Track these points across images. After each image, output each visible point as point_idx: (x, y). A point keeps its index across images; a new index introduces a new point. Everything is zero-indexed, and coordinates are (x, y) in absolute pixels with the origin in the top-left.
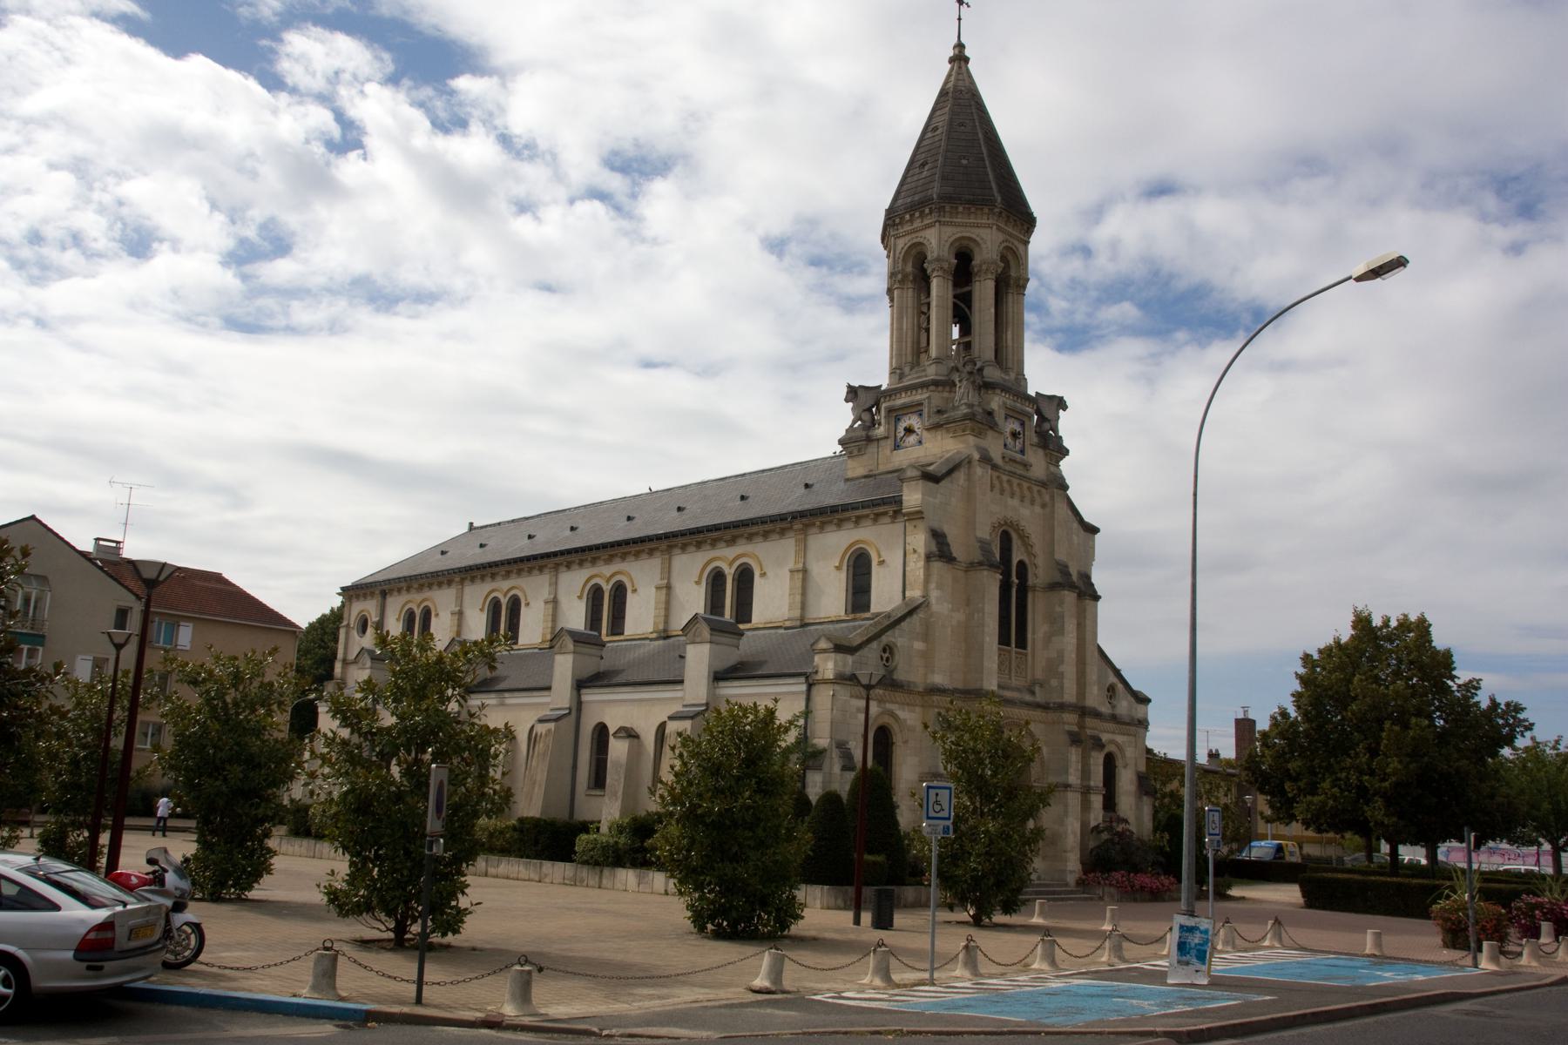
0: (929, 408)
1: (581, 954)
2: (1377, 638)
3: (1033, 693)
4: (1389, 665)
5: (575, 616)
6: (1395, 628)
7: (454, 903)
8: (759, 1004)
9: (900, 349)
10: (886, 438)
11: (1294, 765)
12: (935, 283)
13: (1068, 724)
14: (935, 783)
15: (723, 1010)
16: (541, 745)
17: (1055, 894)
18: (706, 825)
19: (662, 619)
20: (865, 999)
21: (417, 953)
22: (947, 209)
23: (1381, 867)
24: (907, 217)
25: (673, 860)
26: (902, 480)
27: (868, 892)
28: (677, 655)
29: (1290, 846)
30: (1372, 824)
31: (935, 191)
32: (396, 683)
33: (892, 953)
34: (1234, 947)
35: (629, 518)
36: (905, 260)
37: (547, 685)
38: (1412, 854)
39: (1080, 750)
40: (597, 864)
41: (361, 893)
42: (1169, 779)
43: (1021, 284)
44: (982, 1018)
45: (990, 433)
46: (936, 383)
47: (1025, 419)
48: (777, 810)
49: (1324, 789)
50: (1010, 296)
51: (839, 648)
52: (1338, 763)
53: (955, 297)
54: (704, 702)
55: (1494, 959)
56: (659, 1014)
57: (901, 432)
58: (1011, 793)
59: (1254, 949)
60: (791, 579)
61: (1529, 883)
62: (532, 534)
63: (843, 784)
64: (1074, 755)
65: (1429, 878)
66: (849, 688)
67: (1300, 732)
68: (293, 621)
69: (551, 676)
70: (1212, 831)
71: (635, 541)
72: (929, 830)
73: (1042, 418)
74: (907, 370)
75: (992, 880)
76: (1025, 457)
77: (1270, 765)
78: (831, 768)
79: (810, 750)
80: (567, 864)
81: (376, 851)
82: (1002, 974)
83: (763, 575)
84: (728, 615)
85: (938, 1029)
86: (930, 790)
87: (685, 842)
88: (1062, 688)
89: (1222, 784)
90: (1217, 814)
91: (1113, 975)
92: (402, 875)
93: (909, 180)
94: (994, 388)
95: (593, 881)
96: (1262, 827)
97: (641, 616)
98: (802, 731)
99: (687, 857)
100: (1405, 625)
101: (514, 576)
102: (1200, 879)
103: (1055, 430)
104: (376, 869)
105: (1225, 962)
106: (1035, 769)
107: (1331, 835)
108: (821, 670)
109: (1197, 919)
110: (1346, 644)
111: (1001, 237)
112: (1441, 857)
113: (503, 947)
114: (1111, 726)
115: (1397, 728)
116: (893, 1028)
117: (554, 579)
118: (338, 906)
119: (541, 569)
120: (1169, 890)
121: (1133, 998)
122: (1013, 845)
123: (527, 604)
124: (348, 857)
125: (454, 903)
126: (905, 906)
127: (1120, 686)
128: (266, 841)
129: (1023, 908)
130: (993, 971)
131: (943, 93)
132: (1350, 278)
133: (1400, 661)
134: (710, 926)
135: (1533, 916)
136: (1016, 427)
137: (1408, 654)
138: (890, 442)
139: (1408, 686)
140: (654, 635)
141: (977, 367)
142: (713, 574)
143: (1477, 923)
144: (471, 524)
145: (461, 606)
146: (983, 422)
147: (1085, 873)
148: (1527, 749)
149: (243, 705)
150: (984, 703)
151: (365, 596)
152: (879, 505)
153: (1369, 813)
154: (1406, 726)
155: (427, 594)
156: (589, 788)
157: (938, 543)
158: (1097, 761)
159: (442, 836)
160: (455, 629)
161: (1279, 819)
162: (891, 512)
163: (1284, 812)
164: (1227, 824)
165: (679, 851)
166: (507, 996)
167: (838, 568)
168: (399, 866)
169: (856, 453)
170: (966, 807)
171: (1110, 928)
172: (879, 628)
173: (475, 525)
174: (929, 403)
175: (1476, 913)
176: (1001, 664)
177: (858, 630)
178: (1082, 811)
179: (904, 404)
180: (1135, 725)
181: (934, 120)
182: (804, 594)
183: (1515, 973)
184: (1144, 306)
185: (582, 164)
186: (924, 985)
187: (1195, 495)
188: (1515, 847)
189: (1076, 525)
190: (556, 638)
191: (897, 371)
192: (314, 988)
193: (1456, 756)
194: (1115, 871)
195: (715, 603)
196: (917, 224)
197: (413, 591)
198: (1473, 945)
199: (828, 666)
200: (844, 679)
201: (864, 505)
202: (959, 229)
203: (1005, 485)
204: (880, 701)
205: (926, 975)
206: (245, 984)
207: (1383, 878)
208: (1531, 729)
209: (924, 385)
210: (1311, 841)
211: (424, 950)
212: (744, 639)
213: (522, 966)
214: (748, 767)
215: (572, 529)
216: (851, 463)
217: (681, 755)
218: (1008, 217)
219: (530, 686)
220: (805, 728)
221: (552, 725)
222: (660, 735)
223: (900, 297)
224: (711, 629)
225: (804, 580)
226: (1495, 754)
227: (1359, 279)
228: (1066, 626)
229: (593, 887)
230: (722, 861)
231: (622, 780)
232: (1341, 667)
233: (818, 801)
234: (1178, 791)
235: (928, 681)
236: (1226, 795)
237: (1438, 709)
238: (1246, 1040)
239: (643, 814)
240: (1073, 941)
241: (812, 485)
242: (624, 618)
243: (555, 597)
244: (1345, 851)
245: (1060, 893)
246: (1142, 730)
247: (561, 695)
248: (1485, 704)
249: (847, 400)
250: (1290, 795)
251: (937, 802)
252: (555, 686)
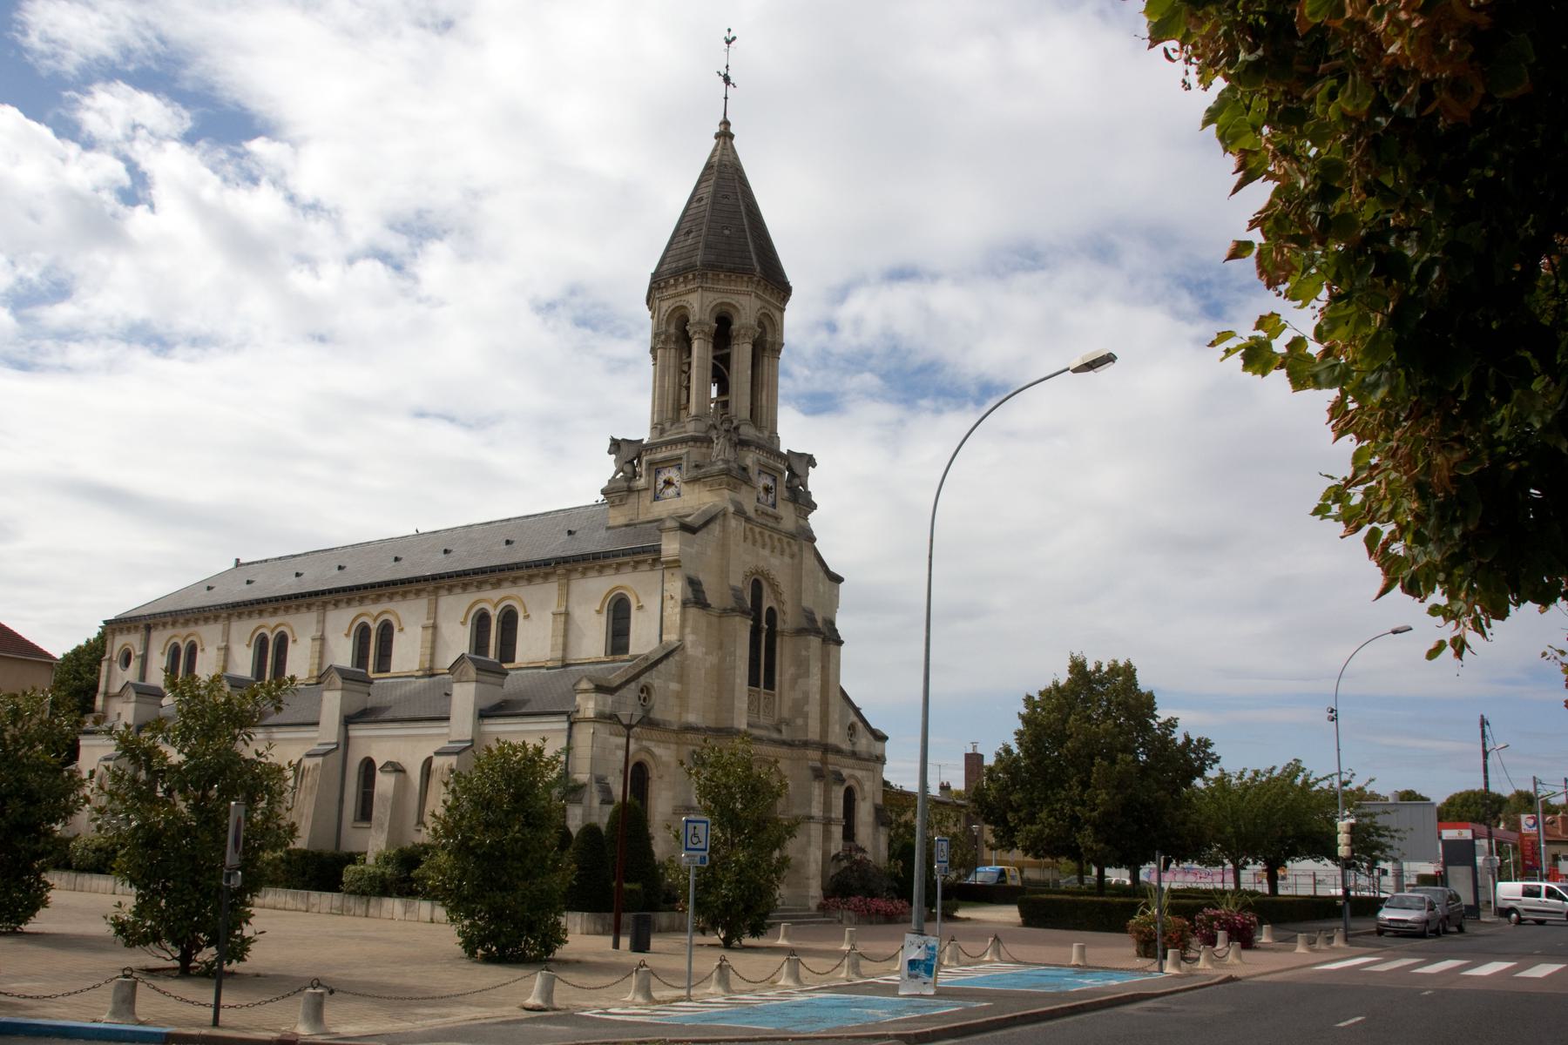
0: (688, 462)
1: (359, 979)
2: (1090, 681)
3: (780, 731)
4: (1100, 706)
5: (342, 653)
6: (1106, 673)
7: (238, 932)
8: (533, 1020)
9: (661, 405)
10: (647, 489)
11: (1015, 797)
12: (696, 345)
13: (812, 760)
14: (692, 817)
15: (501, 1026)
16: (309, 779)
17: (799, 919)
18: (477, 857)
19: (428, 658)
20: (629, 1014)
21: (214, 981)
22: (710, 275)
23: (1090, 888)
24: (672, 281)
25: (445, 889)
26: (661, 531)
27: (627, 918)
28: (443, 692)
29: (1011, 870)
30: (1082, 850)
31: (698, 258)
32: (185, 722)
33: (652, 972)
34: (958, 961)
35: (397, 559)
36: (668, 323)
37: (315, 720)
38: (1118, 876)
39: (822, 784)
40: (364, 894)
41: (148, 923)
42: (904, 811)
43: (777, 348)
44: (735, 1028)
45: (744, 488)
46: (695, 439)
47: (777, 475)
48: (544, 842)
49: (1041, 819)
50: (766, 359)
51: (600, 689)
52: (1054, 795)
53: (715, 358)
54: (470, 738)
55: (1176, 965)
56: (442, 1031)
57: (661, 484)
58: (760, 826)
59: (976, 964)
60: (554, 621)
61: (1211, 898)
62: (300, 572)
63: (602, 817)
64: (817, 790)
65: (1130, 896)
66: (608, 726)
67: (1021, 767)
68: (50, 652)
69: (319, 712)
70: (940, 859)
71: (403, 582)
72: (687, 860)
73: (793, 474)
74: (667, 425)
75: (742, 906)
76: (776, 511)
77: (994, 798)
78: (591, 801)
79: (571, 784)
80: (335, 894)
81: (164, 883)
82: (753, 991)
83: (527, 617)
84: (492, 655)
85: (698, 1038)
86: (689, 824)
87: (457, 872)
88: (807, 725)
89: (952, 814)
90: (945, 843)
91: (851, 988)
92: (190, 906)
93: (674, 246)
94: (749, 446)
95: (360, 910)
96: (987, 854)
97: (407, 654)
98: (563, 767)
99: (459, 887)
100: (1114, 670)
101: (281, 612)
102: (929, 902)
103: (805, 485)
104: (164, 901)
105: (951, 975)
106: (781, 804)
107: (1048, 860)
108: (582, 709)
109: (925, 938)
110: (1064, 687)
111: (758, 304)
112: (1143, 877)
113: (286, 973)
114: (851, 762)
115: (1105, 763)
116: (657, 1038)
117: (321, 618)
118: (126, 937)
119: (309, 607)
120: (902, 913)
121: (868, 1007)
122: (762, 874)
123: (295, 641)
124: (134, 889)
125: (238, 932)
126: (660, 931)
127: (860, 725)
128: (43, 875)
129: (768, 931)
130: (743, 988)
131: (709, 166)
132: (1068, 369)
133: (1110, 702)
134: (480, 951)
135: (1212, 927)
136: (769, 483)
137: (1117, 697)
138: (650, 494)
139: (1116, 725)
140: (420, 673)
141: (734, 425)
142: (477, 616)
143: (1164, 934)
144: (238, 560)
145: (228, 641)
146: (738, 477)
147: (826, 897)
148: (1216, 780)
149: (22, 742)
150: (737, 741)
151: (129, 630)
152: (639, 553)
153: (1079, 841)
154: (1113, 762)
155: (192, 629)
156: (355, 820)
157: (693, 590)
158: (838, 794)
159: (238, 869)
160: (221, 664)
161: (1002, 847)
162: (650, 561)
163: (1006, 840)
164: (956, 851)
165: (451, 879)
166: (300, 1017)
167: (599, 612)
168: (187, 898)
169: (617, 502)
170: (718, 838)
171: (849, 948)
172: (637, 670)
173: (241, 561)
174: (688, 457)
175: (1163, 926)
176: (750, 703)
177: (618, 671)
178: (823, 842)
179: (664, 458)
180: (874, 761)
181: (700, 191)
182: (566, 635)
183: (1192, 975)
184: (885, 377)
185: (363, 227)
186: (682, 1001)
187: (930, 557)
188: (1203, 867)
189: (822, 574)
190: (322, 678)
191: (658, 427)
192: (114, 1013)
193: (1155, 787)
194: (854, 896)
195: (480, 643)
196: (681, 288)
197: (179, 625)
198: (1159, 953)
199: (588, 705)
200: (603, 718)
201: (624, 553)
202: (719, 295)
203: (757, 536)
204: (637, 739)
205: (683, 993)
206: (41, 1012)
207: (1090, 898)
208: (1218, 762)
209: (683, 441)
210: (1031, 866)
211: (215, 976)
212: (508, 678)
213: (314, 988)
214: (517, 802)
215: (340, 568)
216: (612, 512)
217: (454, 791)
218: (766, 286)
219: (298, 721)
220: (567, 764)
221: (319, 760)
222: (426, 767)
223: (663, 356)
224: (477, 669)
225: (567, 622)
226: (1188, 785)
227: (1075, 371)
228: (811, 668)
229: (360, 916)
230: (491, 889)
231: (389, 812)
232: (1059, 708)
233: (579, 832)
234: (912, 822)
235: (683, 720)
236: (955, 825)
237: (1141, 745)
238: (964, 1040)
239: (409, 845)
240: (816, 960)
241: (575, 532)
242: (390, 656)
243: (323, 635)
244: (1061, 875)
245: (803, 917)
246: (879, 765)
247: (329, 730)
248: (1180, 741)
249: (610, 452)
250: (1012, 825)
251: (695, 835)
252: (323, 721)
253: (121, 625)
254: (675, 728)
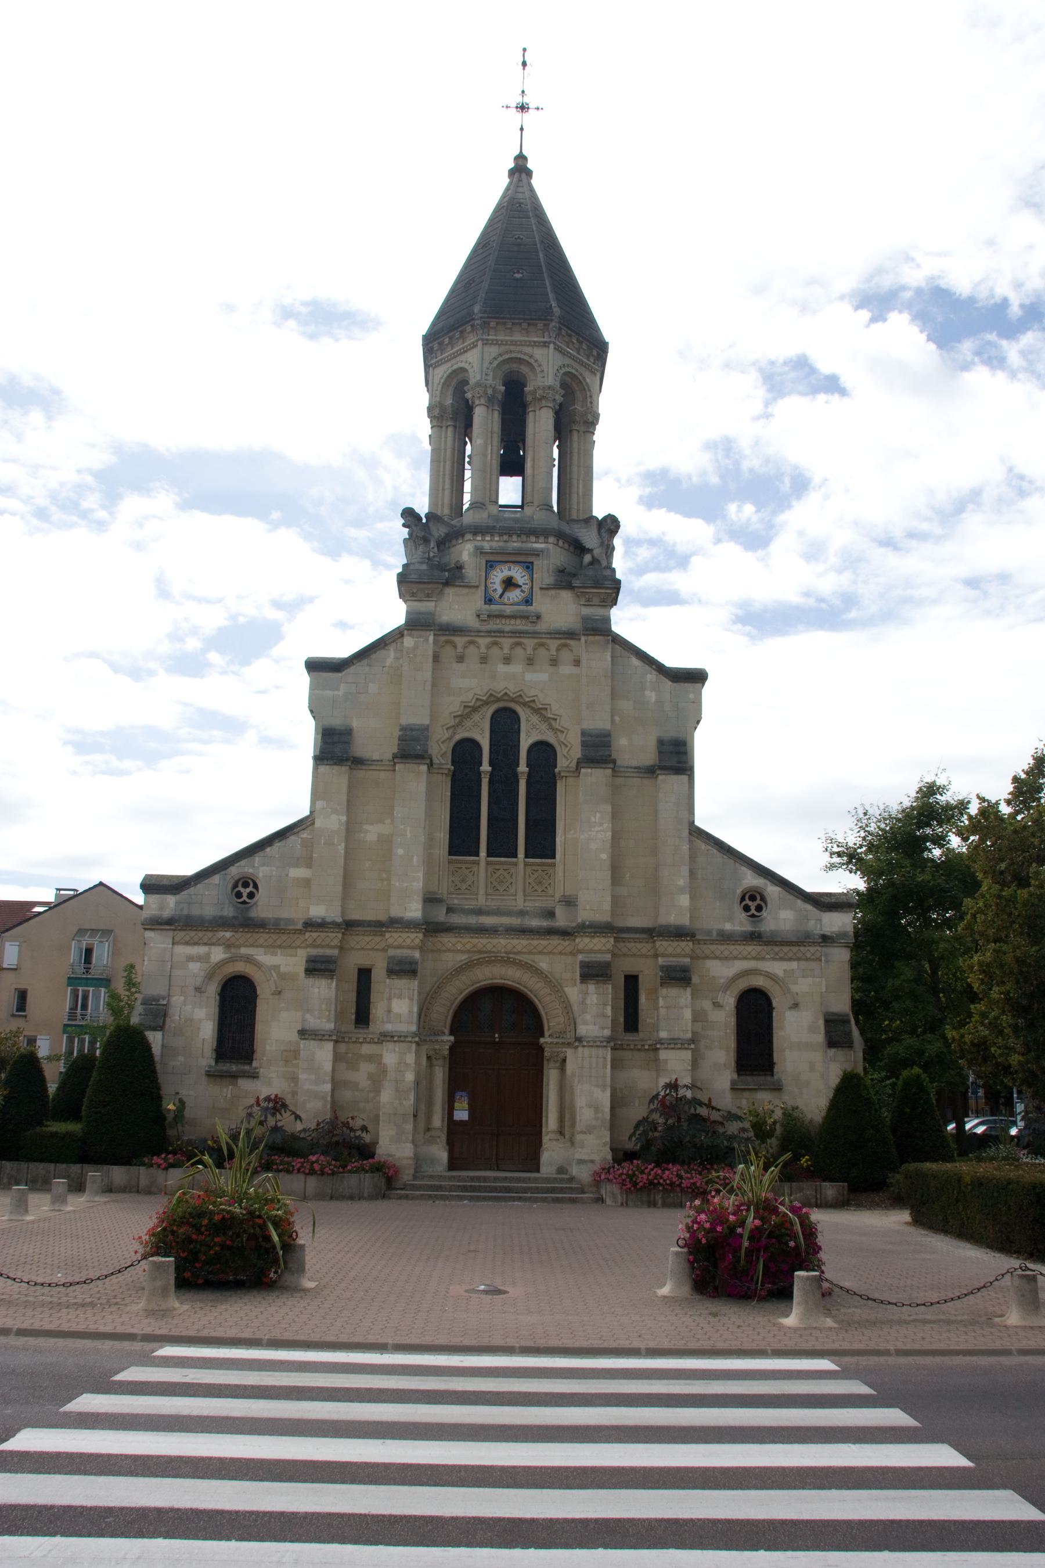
66: (171, 933)
94: (463, 536)
254: (300, 926)
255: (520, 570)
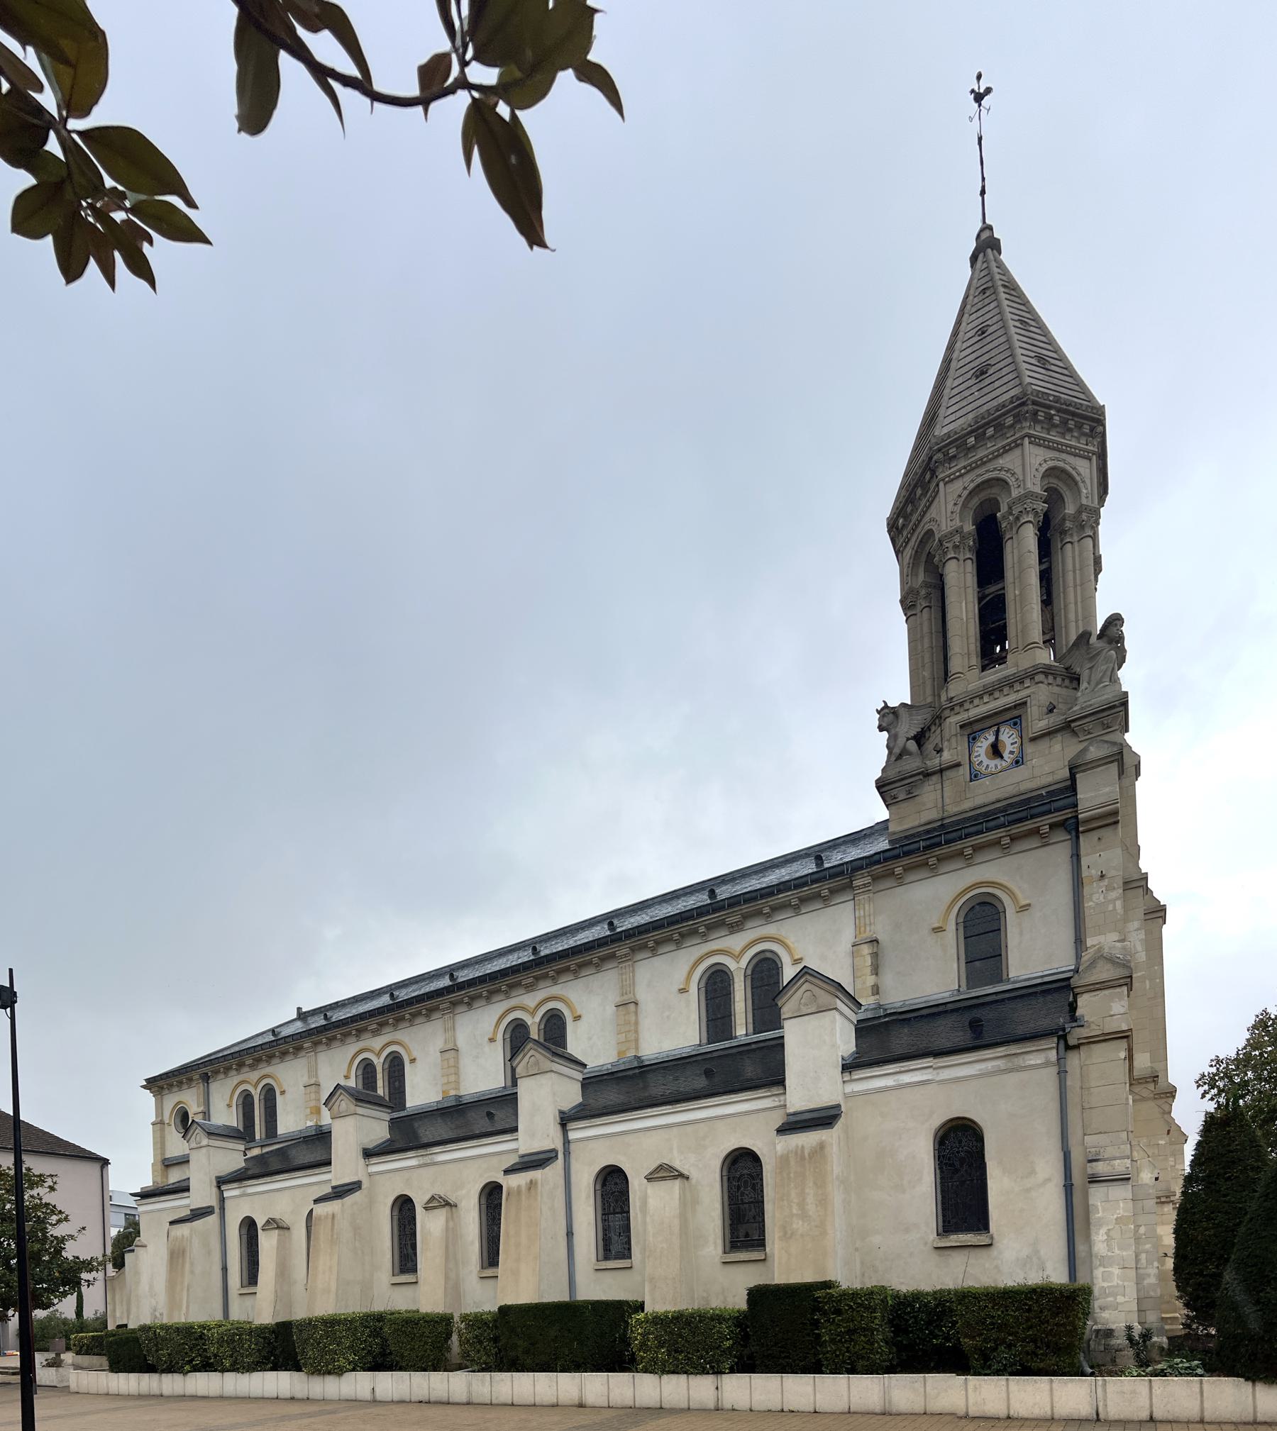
156: (483, 1268)
253: (169, 1081)
255: (1007, 730)
